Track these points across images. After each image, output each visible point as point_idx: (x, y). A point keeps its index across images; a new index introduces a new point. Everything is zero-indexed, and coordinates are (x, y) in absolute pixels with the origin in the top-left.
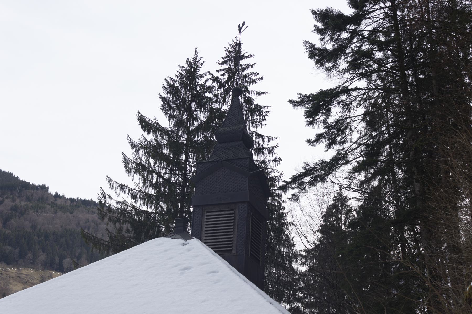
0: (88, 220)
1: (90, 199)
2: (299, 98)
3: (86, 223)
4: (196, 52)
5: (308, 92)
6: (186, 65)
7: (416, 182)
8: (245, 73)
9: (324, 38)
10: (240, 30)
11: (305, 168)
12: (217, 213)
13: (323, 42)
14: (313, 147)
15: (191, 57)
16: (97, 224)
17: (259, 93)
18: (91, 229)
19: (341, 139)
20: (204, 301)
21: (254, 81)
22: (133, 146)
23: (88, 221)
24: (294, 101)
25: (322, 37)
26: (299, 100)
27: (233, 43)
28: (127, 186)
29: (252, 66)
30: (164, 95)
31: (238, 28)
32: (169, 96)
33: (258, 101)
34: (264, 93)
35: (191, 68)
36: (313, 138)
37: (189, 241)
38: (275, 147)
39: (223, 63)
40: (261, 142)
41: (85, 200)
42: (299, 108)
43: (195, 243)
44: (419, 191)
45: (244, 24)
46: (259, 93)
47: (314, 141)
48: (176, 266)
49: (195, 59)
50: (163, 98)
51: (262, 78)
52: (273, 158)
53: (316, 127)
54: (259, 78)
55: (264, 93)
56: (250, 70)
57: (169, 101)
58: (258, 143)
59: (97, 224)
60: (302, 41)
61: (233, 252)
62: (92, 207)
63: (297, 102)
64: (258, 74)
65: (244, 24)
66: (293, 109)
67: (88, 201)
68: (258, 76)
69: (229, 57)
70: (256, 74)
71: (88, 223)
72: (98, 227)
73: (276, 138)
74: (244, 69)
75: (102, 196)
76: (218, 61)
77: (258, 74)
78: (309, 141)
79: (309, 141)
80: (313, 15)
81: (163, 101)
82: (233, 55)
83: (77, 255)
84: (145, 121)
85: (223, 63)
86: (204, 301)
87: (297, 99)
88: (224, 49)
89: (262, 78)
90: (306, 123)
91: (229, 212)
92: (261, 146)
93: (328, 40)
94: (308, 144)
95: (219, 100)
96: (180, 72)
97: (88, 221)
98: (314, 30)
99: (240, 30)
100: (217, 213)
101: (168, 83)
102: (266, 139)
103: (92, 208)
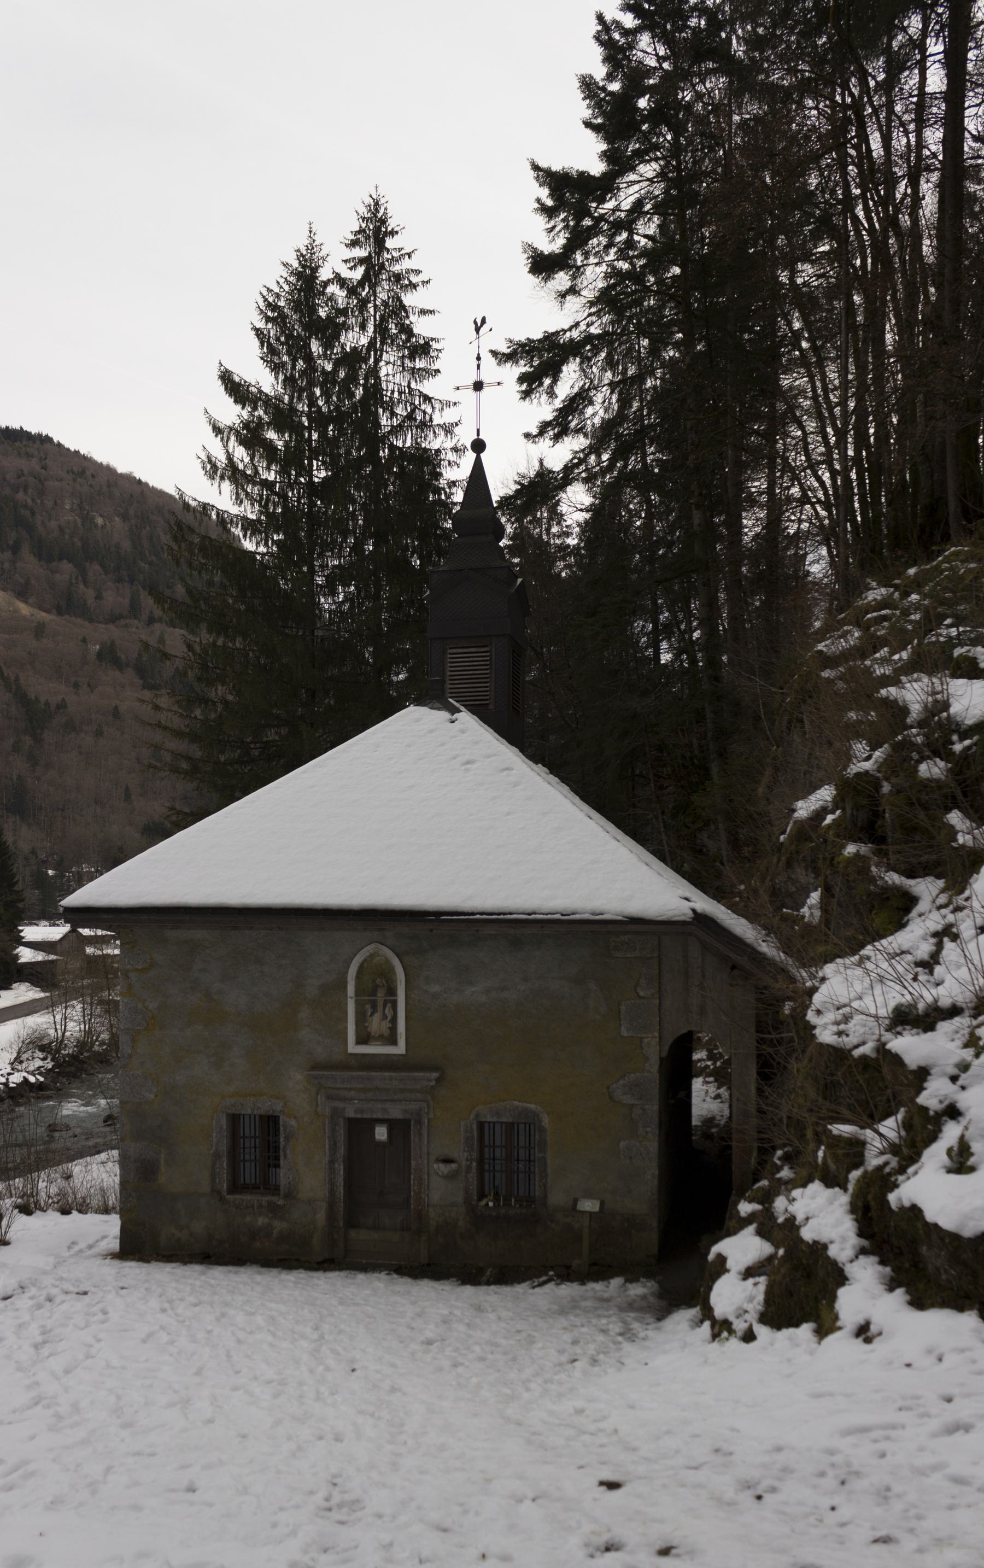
0: (22, 471)
1: (18, 427)
2: (509, 347)
3: (19, 477)
4: (311, 232)
5: (521, 337)
6: (295, 264)
7: (696, 509)
8: (397, 268)
9: (554, 227)
10: (477, 330)
11: (519, 483)
12: (465, 650)
13: (552, 234)
14: (533, 445)
15: (302, 242)
16: (40, 481)
17: (423, 312)
18: (30, 491)
19: (578, 425)
20: (508, 814)
21: (414, 286)
22: (217, 430)
23: (20, 474)
24: (499, 353)
25: (550, 226)
26: (508, 351)
27: (372, 201)
28: (213, 506)
29: (409, 255)
30: (261, 325)
31: (474, 326)
32: (270, 325)
33: (422, 327)
34: (432, 312)
35: (304, 267)
36: (535, 431)
37: (456, 715)
38: (457, 425)
39: (354, 244)
40: (429, 410)
41: (7, 428)
42: (508, 365)
43: (466, 718)
44: (699, 525)
45: (484, 321)
46: (423, 312)
47: (536, 436)
48: (454, 758)
49: (311, 248)
50: (258, 332)
51: (428, 282)
52: (452, 445)
53: (535, 401)
54: (423, 282)
55: (432, 312)
56: (406, 264)
57: (269, 337)
58: (425, 412)
59: (40, 481)
60: (520, 244)
61: (491, 707)
62: (24, 443)
63: (504, 354)
64: (420, 272)
65: (484, 321)
66: (498, 367)
67: (15, 431)
68: (422, 277)
69: (364, 231)
70: (417, 272)
71: (23, 478)
72: (43, 485)
73: (455, 404)
74: (394, 260)
75: (175, 528)
76: (344, 241)
77: (420, 272)
78: (527, 436)
79: (527, 436)
80: (532, 172)
81: (258, 335)
82: (371, 227)
83: (11, 542)
84: (233, 382)
85: (354, 244)
86: (508, 814)
87: (504, 349)
88: (356, 217)
89: (428, 282)
90: (519, 396)
91: (482, 650)
92: (428, 418)
93: (560, 231)
94: (525, 441)
95: (349, 322)
96: (285, 275)
97: (23, 475)
98: (536, 210)
99: (477, 330)
100: (465, 650)
101: (266, 300)
102: (437, 405)
103: (25, 446)
